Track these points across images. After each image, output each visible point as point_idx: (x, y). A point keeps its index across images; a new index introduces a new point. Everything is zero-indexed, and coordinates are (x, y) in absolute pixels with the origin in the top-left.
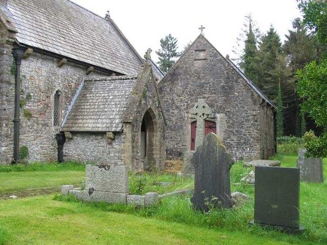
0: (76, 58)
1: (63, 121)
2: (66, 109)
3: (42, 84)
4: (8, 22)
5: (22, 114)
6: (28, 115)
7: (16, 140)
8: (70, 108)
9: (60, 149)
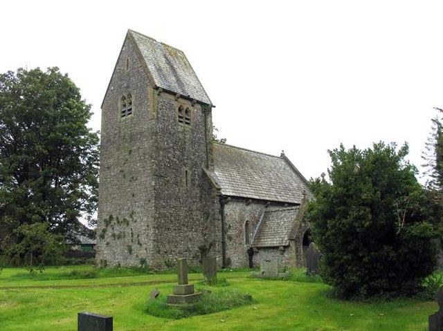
0: (258, 198)
1: (252, 241)
2: (253, 233)
3: (237, 218)
4: (217, 183)
5: (226, 237)
6: (230, 238)
7: (224, 254)
8: (256, 231)
9: (251, 259)
